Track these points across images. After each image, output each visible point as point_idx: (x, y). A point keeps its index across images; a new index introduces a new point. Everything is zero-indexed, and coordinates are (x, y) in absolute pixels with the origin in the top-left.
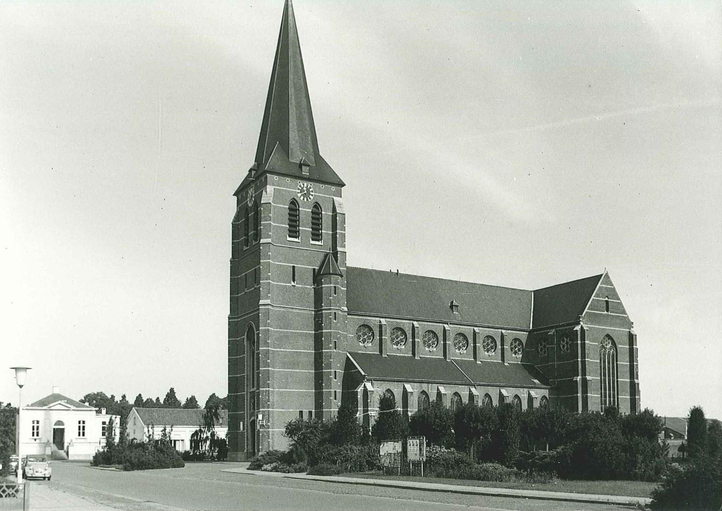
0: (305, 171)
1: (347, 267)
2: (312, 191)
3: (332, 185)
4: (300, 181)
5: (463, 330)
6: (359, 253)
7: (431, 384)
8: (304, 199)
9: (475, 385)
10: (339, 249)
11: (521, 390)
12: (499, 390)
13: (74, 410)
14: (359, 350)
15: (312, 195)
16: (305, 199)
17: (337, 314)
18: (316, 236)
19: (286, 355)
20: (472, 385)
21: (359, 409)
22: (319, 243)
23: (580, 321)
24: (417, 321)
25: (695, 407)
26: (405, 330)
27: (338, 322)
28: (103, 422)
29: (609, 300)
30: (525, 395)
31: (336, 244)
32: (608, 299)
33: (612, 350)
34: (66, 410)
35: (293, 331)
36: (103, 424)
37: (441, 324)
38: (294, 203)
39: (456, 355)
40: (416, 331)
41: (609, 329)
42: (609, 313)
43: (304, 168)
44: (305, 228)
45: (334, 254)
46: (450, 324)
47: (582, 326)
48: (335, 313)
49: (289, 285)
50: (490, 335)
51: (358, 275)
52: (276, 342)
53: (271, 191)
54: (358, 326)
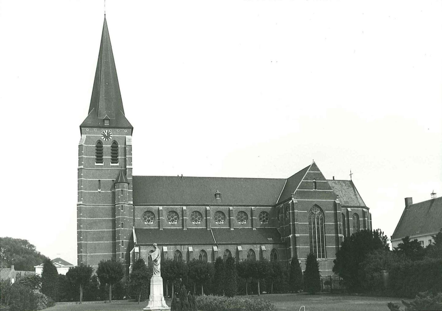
0: (107, 123)
1: (133, 177)
2: (111, 134)
3: (125, 129)
4: (103, 129)
5: (198, 209)
6: (141, 167)
7: (183, 246)
8: (106, 140)
9: (217, 245)
10: (127, 167)
11: (255, 246)
12: (236, 247)
13: (63, 267)
15: (111, 137)
16: (107, 139)
17: (123, 206)
18: (115, 160)
19: (94, 233)
20: (215, 245)
21: (131, 264)
23: (292, 197)
24: (186, 206)
25: (427, 246)
26: (178, 212)
27: (124, 211)
29: (316, 181)
30: (258, 249)
31: (126, 164)
32: (316, 180)
33: (321, 215)
34: (59, 267)
35: (99, 219)
37: (204, 207)
38: (100, 143)
39: (216, 226)
40: (184, 212)
42: (317, 190)
43: (105, 121)
44: (107, 157)
45: (125, 171)
46: (211, 206)
47: (293, 201)
49: (97, 191)
50: (242, 210)
51: (141, 183)
52: (88, 226)
53: (84, 137)
54: (143, 213)
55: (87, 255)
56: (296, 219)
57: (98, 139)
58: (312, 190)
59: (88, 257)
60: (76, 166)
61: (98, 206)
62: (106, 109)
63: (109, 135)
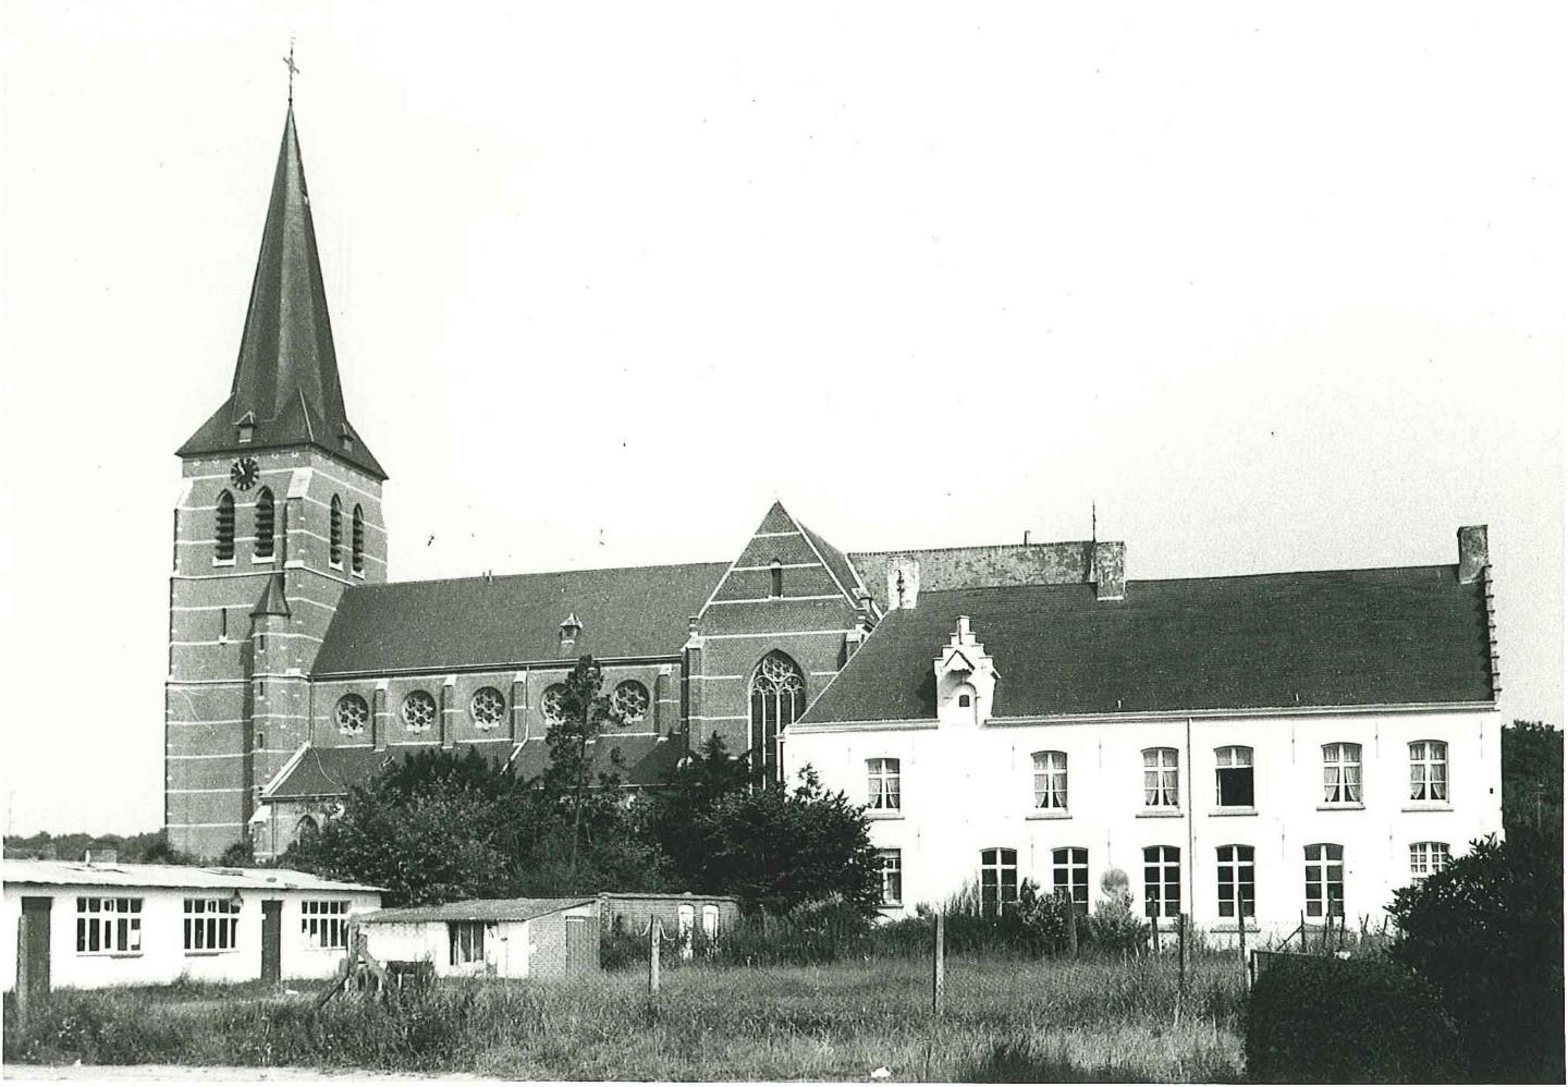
14: (339, 744)
19: (209, 765)
22: (232, 562)
28: (1251, 849)
29: (783, 567)
36: (985, 862)
41: (774, 637)
44: (245, 539)
48: (261, 683)
55: (188, 829)
56: (694, 704)
57: (222, 489)
58: (765, 600)
59: (191, 836)
60: (711, 560)
61: (216, 687)
62: (286, 392)
63: (248, 469)
